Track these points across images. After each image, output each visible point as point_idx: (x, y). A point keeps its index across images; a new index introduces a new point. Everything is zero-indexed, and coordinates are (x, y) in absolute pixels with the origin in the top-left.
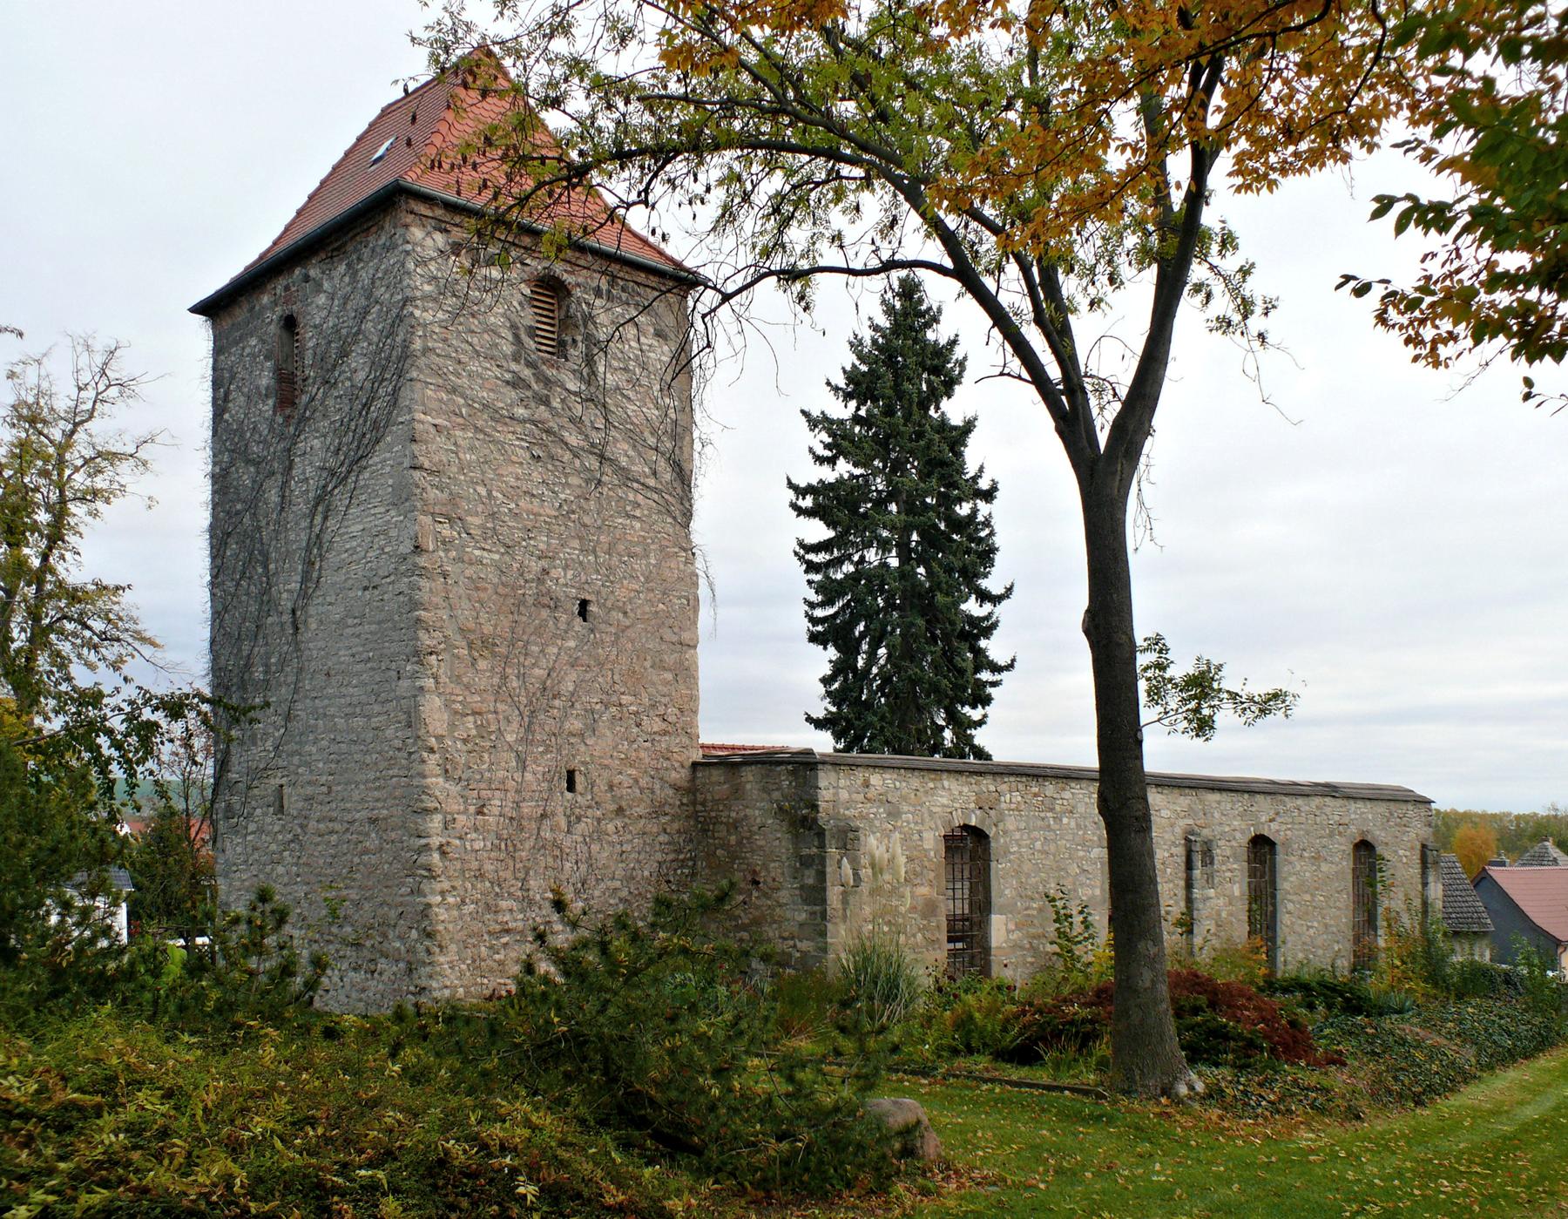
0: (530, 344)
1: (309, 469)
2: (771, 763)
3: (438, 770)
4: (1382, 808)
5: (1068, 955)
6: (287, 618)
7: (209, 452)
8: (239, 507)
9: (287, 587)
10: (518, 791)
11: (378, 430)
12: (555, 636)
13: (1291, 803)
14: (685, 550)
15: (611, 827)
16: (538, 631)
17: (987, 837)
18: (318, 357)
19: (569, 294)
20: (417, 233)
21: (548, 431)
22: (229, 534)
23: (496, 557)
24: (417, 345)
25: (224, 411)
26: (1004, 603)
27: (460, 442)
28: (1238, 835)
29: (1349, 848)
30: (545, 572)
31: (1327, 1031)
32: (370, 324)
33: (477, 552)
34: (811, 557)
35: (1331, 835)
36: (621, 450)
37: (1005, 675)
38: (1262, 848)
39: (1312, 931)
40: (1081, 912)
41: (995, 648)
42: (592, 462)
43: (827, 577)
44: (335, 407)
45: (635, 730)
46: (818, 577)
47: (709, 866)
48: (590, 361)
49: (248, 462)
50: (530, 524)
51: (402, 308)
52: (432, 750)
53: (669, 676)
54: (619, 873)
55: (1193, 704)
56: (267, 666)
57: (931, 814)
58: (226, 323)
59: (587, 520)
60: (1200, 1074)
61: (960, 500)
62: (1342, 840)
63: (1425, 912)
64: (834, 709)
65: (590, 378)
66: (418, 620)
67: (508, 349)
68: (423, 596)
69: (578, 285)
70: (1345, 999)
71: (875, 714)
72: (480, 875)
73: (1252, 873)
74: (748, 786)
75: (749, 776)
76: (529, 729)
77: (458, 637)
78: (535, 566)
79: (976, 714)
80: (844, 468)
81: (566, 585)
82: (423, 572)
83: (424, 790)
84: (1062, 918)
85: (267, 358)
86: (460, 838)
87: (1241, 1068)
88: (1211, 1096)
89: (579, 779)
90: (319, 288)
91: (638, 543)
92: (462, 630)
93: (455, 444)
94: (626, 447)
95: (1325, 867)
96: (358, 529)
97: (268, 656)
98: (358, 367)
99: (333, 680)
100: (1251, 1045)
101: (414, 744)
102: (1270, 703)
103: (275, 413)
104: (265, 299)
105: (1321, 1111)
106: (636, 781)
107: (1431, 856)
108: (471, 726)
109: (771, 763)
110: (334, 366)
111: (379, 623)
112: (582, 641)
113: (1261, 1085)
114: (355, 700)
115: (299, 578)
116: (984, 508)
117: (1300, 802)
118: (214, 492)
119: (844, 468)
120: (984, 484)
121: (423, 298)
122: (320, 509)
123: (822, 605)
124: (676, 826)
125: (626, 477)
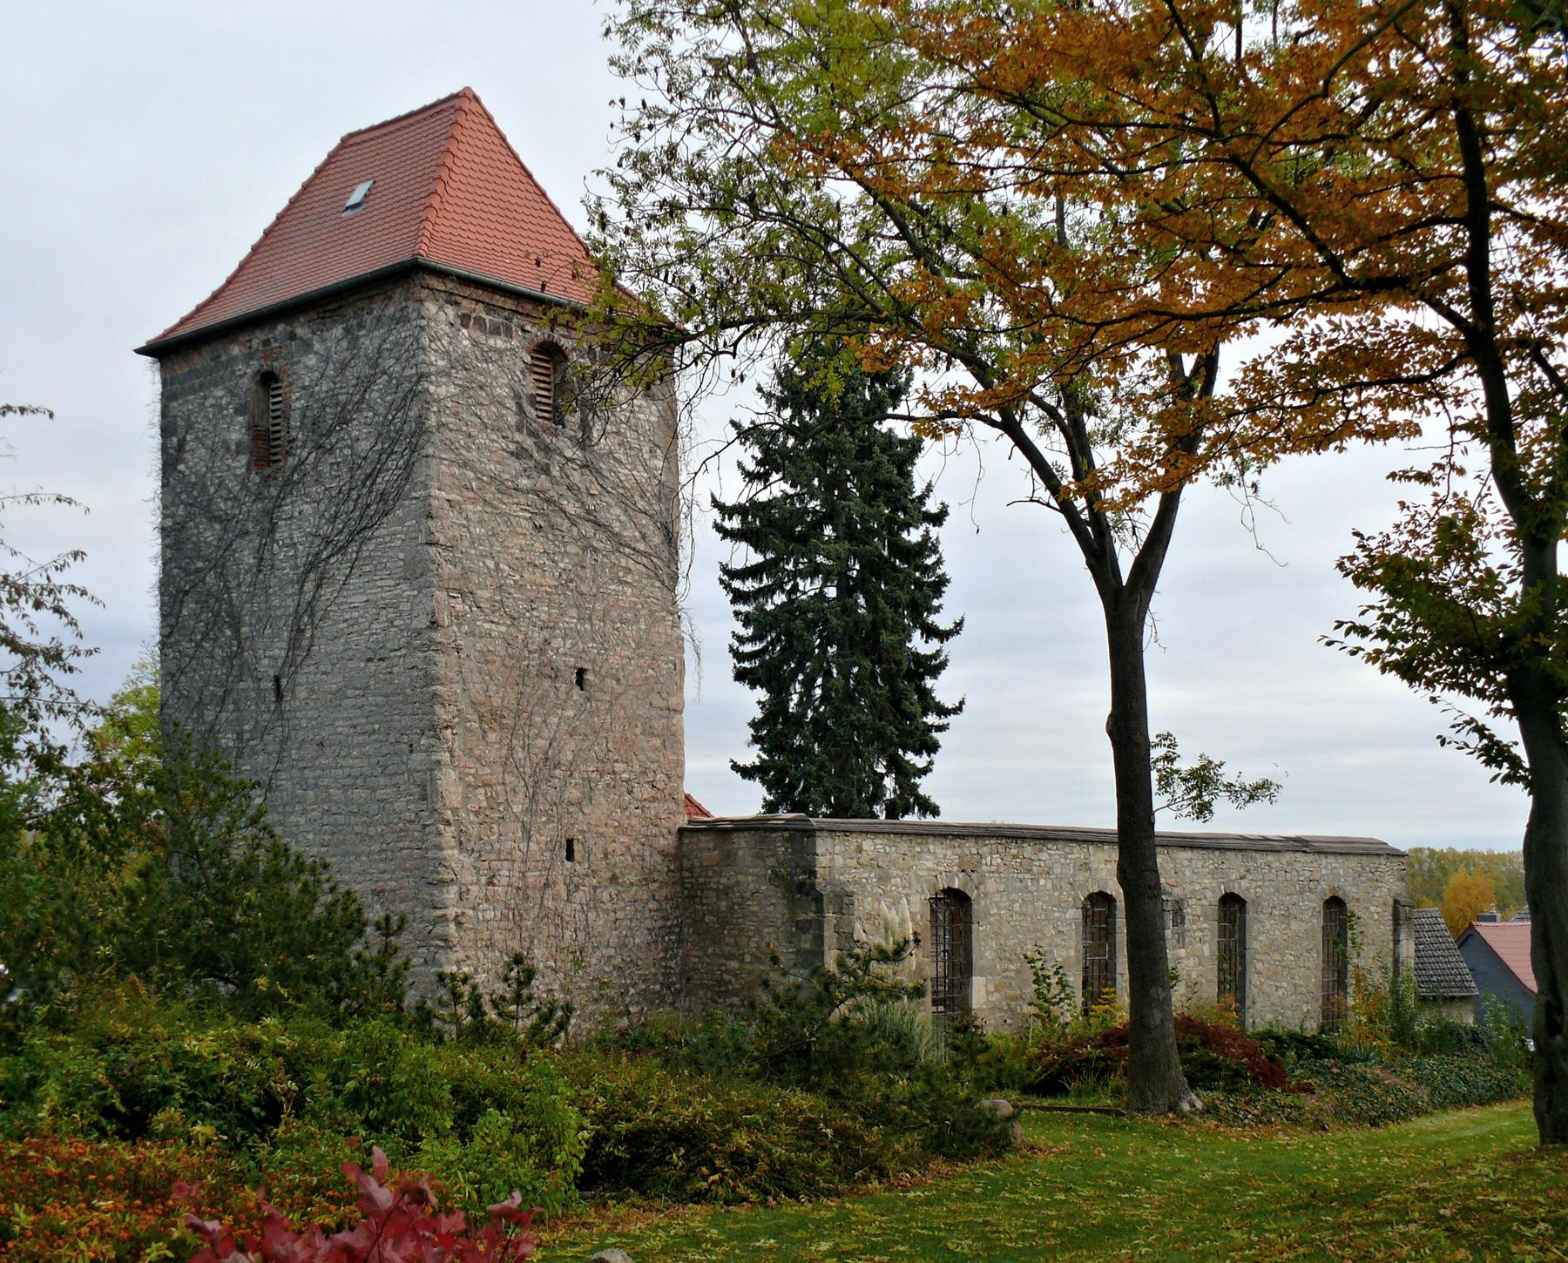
0: (531, 412)
1: (296, 534)
2: (765, 830)
3: (453, 843)
4: (1353, 862)
5: (1047, 1018)
6: (269, 685)
7: (158, 503)
8: (200, 564)
9: (269, 654)
10: (524, 862)
11: (386, 503)
12: (555, 706)
13: (1261, 859)
14: (672, 614)
15: (605, 896)
16: (541, 702)
17: (968, 899)
18: (308, 421)
19: (566, 358)
20: (431, 308)
21: (549, 501)
22: (186, 593)
23: (503, 629)
24: (432, 421)
25: (179, 460)
26: (953, 640)
27: (471, 515)
28: (1209, 894)
29: (1319, 905)
30: (547, 642)
31: (1297, 1072)
32: (375, 395)
33: (487, 626)
34: (736, 584)
35: (1301, 893)
36: (614, 515)
37: (952, 719)
38: (1232, 905)
39: (1280, 992)
40: (1056, 973)
41: (942, 688)
42: (588, 529)
43: (761, 609)
44: (332, 475)
45: (627, 797)
46: (744, 608)
47: (697, 933)
48: (585, 426)
49: (213, 518)
50: (532, 595)
51: (418, 381)
52: (448, 823)
53: (658, 742)
54: (614, 941)
55: (1194, 794)
56: (240, 734)
57: (918, 877)
58: (182, 369)
59: (584, 588)
60: (1198, 1096)
61: (906, 526)
62: (1313, 897)
63: (1396, 972)
64: (765, 756)
65: (584, 443)
66: (435, 694)
67: (512, 419)
68: (440, 671)
69: (574, 349)
70: (1314, 1048)
71: (812, 762)
72: (491, 945)
73: (1222, 932)
74: (740, 853)
75: (742, 842)
76: (533, 799)
77: (470, 711)
78: (538, 637)
79: (920, 761)
80: (778, 487)
81: (565, 654)
82: (439, 648)
83: (441, 862)
84: (1039, 979)
85: (237, 412)
86: (474, 908)
87: (1231, 1092)
88: (1208, 1111)
89: (577, 847)
90: (307, 347)
91: (630, 609)
92: (474, 704)
93: (467, 518)
94: (618, 512)
95: (1294, 925)
96: (359, 602)
97: (240, 722)
98: (361, 435)
99: (327, 750)
100: (1238, 1074)
101: (429, 817)
102: (1260, 790)
103: (248, 469)
104: (236, 350)
105: (1295, 1122)
106: (628, 848)
107: (1403, 912)
108: (482, 797)
109: (765, 830)
110: (328, 435)
111: (387, 696)
112: (580, 710)
113: (1247, 1103)
114: (356, 772)
115: (284, 645)
116: (934, 532)
117: (1270, 858)
118: (165, 547)
119: (778, 487)
120: (931, 506)
121: (438, 373)
122: (312, 576)
123: (752, 639)
124: (664, 892)
125: (618, 542)
